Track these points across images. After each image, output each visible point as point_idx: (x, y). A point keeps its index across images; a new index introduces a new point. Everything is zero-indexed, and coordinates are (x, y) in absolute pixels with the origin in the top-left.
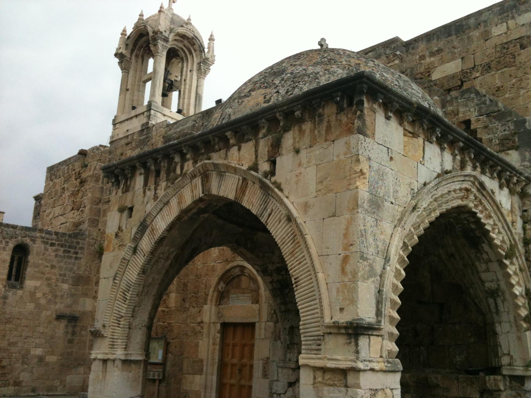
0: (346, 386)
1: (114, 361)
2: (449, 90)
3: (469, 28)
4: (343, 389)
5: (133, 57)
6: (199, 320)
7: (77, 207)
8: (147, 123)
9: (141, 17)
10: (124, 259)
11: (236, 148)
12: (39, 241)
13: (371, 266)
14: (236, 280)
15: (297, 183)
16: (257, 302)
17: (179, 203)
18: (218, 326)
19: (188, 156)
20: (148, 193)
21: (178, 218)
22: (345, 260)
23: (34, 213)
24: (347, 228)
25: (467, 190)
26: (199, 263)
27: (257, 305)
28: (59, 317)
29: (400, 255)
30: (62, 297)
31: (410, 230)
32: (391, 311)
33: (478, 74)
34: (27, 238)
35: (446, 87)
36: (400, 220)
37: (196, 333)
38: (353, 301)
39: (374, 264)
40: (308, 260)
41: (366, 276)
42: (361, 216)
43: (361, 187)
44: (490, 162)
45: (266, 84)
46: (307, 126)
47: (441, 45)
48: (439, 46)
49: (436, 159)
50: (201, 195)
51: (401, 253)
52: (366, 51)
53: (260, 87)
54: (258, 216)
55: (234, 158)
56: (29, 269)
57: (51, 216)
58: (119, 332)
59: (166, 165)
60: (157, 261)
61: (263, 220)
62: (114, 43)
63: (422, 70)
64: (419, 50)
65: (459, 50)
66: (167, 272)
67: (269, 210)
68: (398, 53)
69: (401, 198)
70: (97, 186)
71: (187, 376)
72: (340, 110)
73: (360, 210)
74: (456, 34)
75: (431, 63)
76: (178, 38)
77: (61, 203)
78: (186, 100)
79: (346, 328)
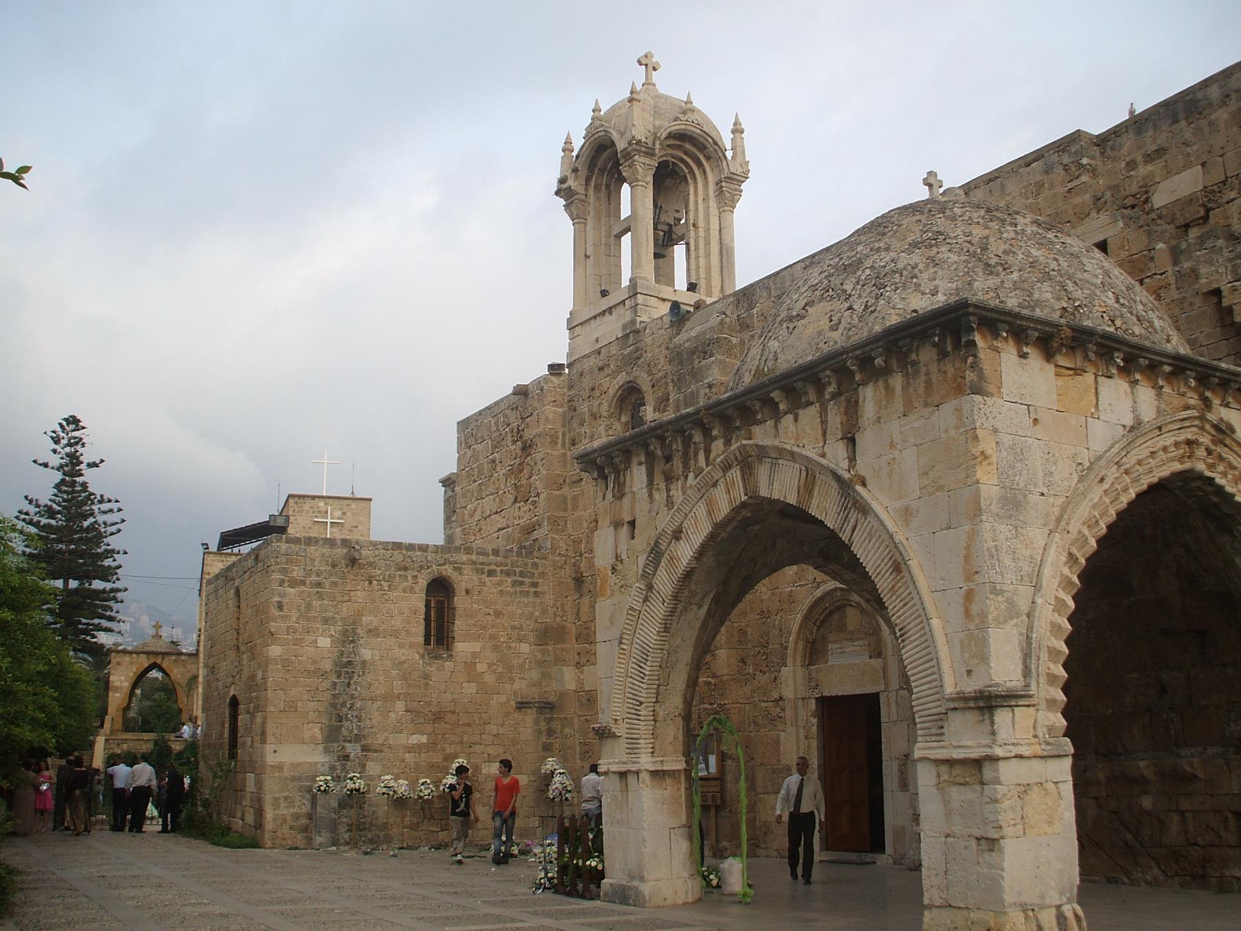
0: (982, 783)
1: (637, 773)
2: (1187, 227)
3: (1210, 105)
4: (978, 788)
5: (591, 192)
6: (775, 695)
7: (522, 496)
8: (633, 322)
9: (597, 114)
10: (632, 609)
11: (790, 417)
12: (467, 569)
13: (1010, 602)
14: (836, 617)
15: (890, 475)
16: (879, 655)
17: (709, 512)
18: (813, 705)
19: (715, 433)
20: (656, 495)
21: (712, 537)
22: (969, 596)
23: (445, 512)
24: (968, 547)
25: (1189, 443)
26: (764, 589)
27: (879, 660)
28: (522, 706)
29: (1062, 575)
30: (521, 667)
31: (1080, 532)
32: (1052, 665)
33: (1233, 195)
34: (446, 567)
35: (1181, 221)
36: (1059, 519)
37: (774, 720)
38: (984, 659)
39: (1015, 598)
40: (916, 600)
41: (1002, 619)
42: (987, 526)
43: (984, 479)
44: (1233, 384)
45: (831, 293)
46: (897, 381)
47: (1162, 139)
48: (1159, 142)
49: (1121, 401)
50: (744, 498)
51: (1066, 571)
52: (1026, 161)
53: (822, 298)
54: (837, 531)
55: (790, 435)
56: (458, 622)
57: (477, 516)
58: (644, 728)
59: (680, 448)
60: (685, 609)
61: (845, 537)
62: (552, 171)
63: (1134, 188)
64: (1125, 150)
65: (1195, 148)
66: (704, 624)
67: (852, 521)
68: (1085, 161)
69: (1060, 483)
70: (556, 453)
71: (765, 796)
72: (943, 355)
73: (984, 518)
74: (1186, 119)
75: (1148, 176)
76: (671, 142)
77: (491, 489)
78: (702, 261)
79: (975, 699)
